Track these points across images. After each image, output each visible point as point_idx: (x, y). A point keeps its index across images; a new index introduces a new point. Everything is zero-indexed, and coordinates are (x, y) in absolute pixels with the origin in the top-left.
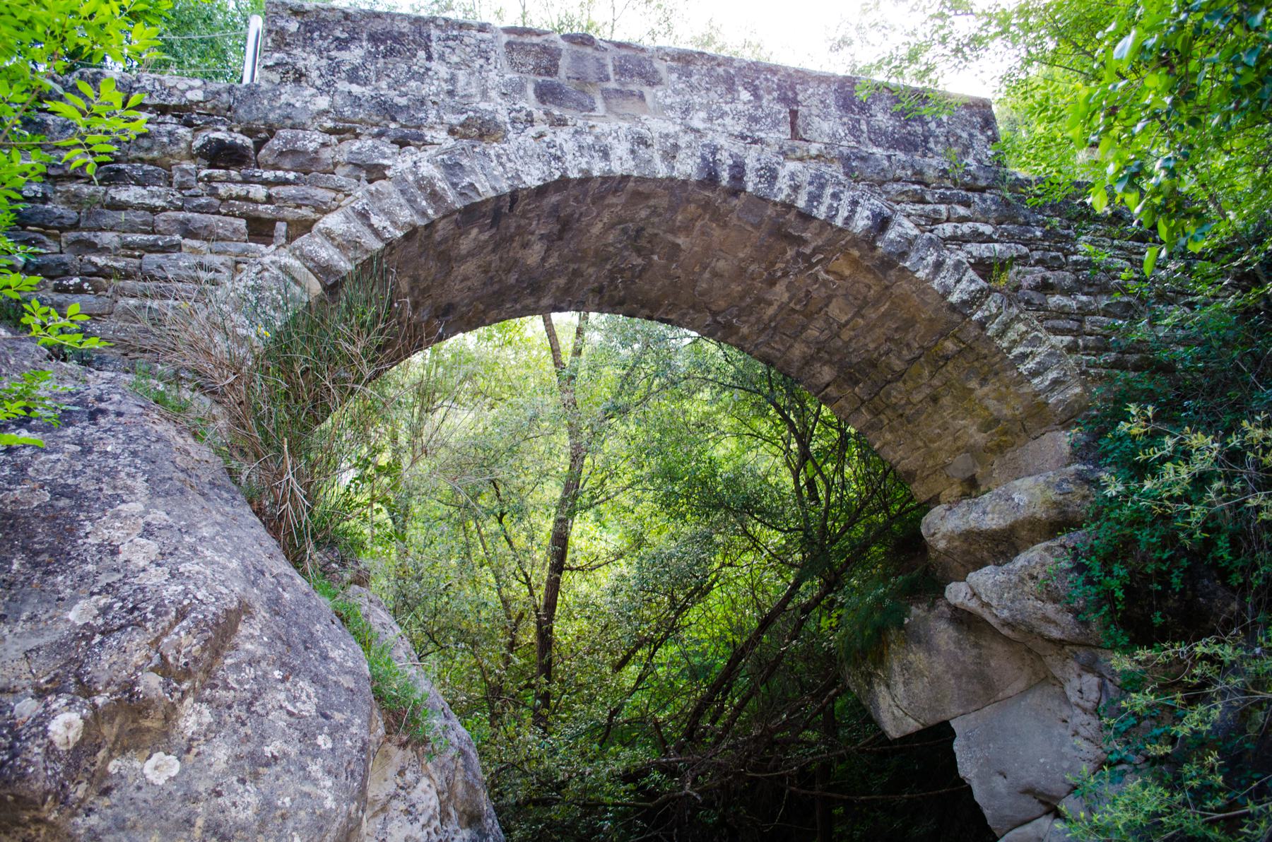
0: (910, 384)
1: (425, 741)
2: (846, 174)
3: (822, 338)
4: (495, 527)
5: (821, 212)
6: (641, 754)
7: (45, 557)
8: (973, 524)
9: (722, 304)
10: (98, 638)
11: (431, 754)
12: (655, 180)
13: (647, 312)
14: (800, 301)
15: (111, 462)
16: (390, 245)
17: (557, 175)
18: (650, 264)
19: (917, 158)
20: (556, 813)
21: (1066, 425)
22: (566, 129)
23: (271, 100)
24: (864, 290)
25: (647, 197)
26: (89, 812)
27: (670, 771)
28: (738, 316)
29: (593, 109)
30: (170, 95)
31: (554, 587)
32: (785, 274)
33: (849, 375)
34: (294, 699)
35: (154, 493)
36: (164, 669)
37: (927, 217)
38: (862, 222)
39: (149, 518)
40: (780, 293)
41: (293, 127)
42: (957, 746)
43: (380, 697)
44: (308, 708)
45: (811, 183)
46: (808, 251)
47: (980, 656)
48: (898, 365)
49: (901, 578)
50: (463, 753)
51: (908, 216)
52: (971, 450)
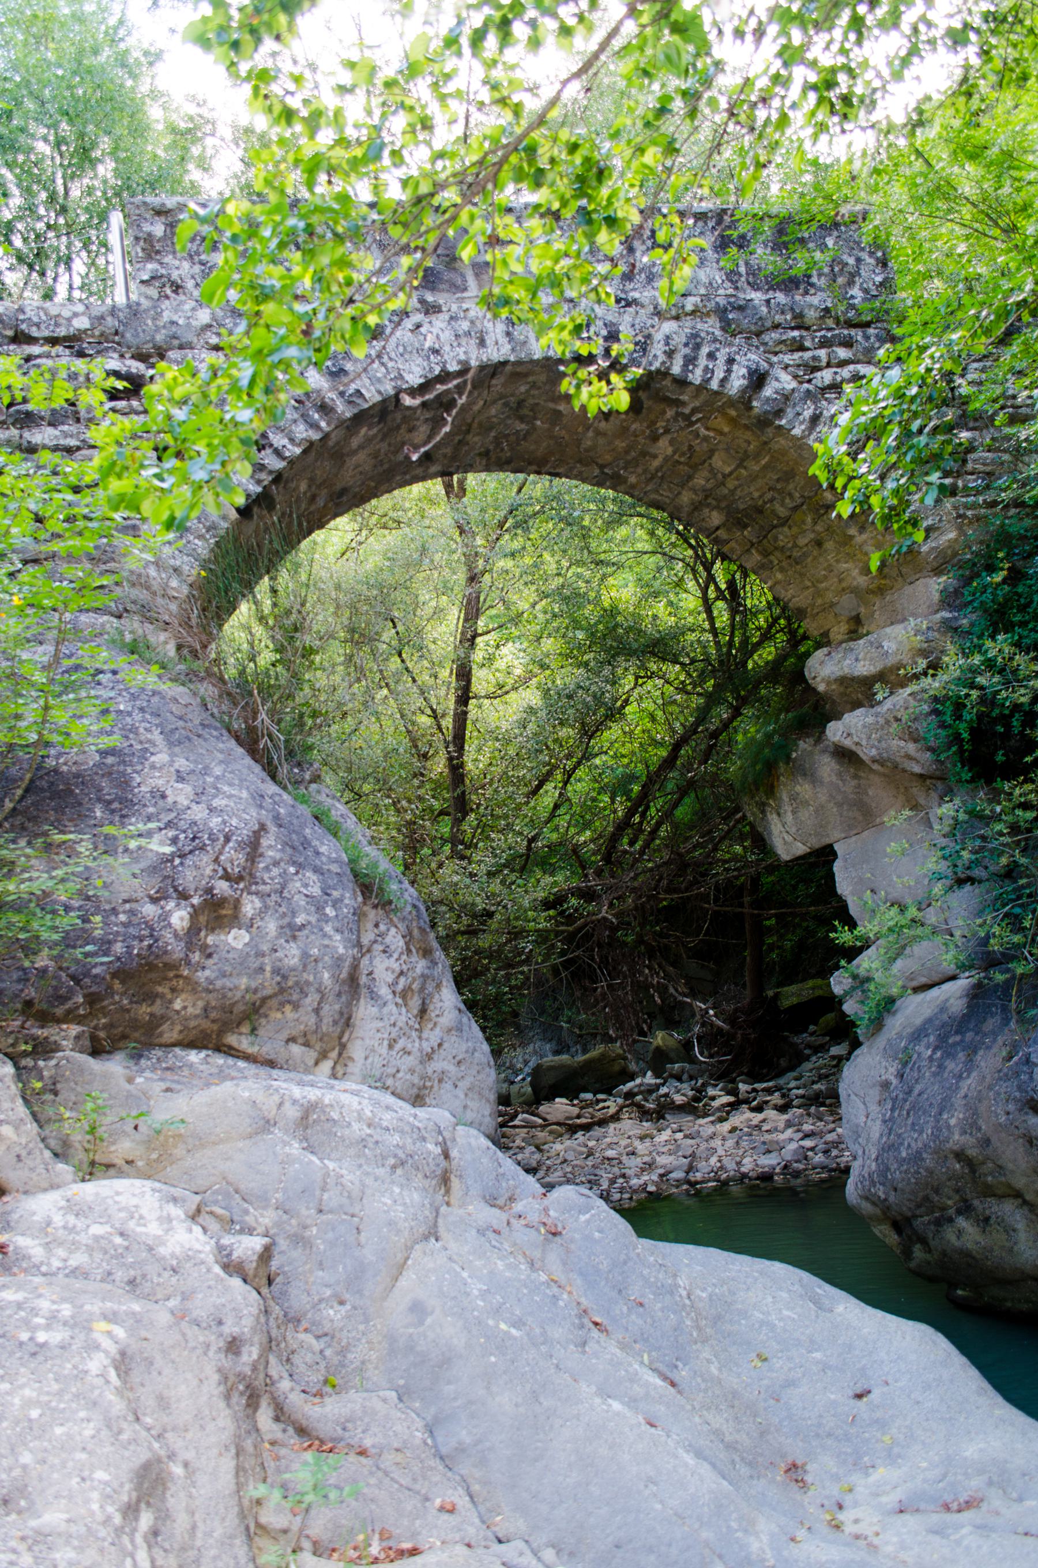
0: (795, 530)
1: (390, 902)
2: (723, 329)
3: (709, 486)
4: (395, 663)
5: (696, 377)
6: (561, 880)
7: (115, 805)
8: (846, 671)
9: (608, 458)
10: (177, 861)
11: (396, 910)
12: (532, 361)
13: (534, 468)
14: (683, 454)
15: (129, 720)
16: (292, 462)
17: (437, 370)
18: (534, 428)
19: (798, 298)
20: (485, 941)
21: (938, 571)
22: (441, 316)
23: (154, 319)
24: (744, 445)
25: (526, 375)
26: (204, 968)
27: (588, 895)
28: (625, 468)
29: (465, 289)
30: (57, 325)
31: (461, 719)
32: (667, 431)
33: (737, 520)
34: (306, 886)
35: (171, 744)
36: (227, 877)
37: (806, 365)
38: (737, 383)
39: (176, 765)
40: (664, 447)
41: (181, 347)
42: (837, 867)
43: (355, 876)
44: (316, 890)
45: (686, 345)
46: (687, 411)
47: (859, 786)
48: (782, 512)
49: (790, 715)
50: (414, 906)
51: (786, 367)
52: (855, 591)
